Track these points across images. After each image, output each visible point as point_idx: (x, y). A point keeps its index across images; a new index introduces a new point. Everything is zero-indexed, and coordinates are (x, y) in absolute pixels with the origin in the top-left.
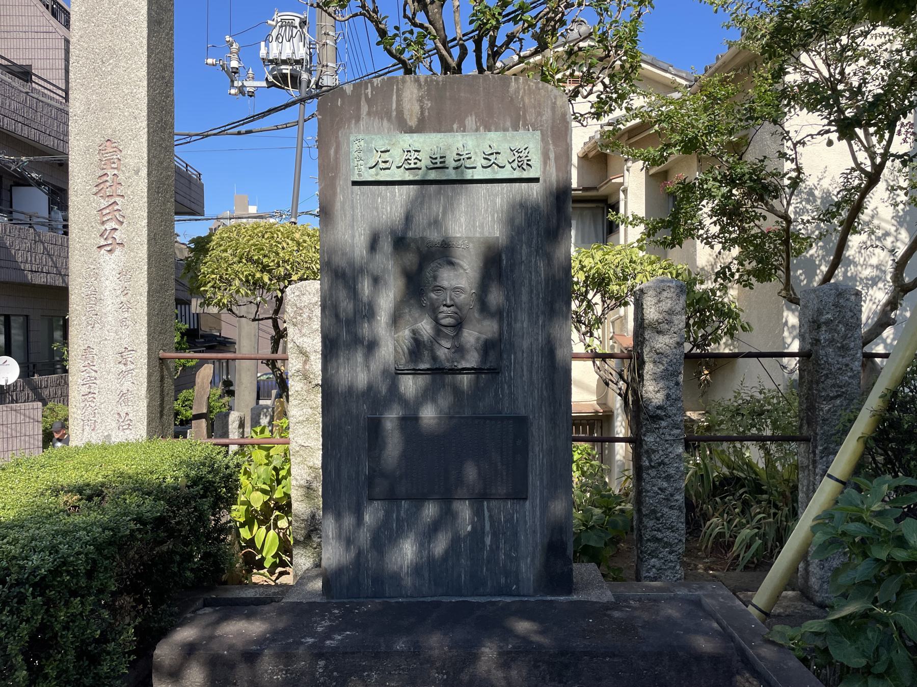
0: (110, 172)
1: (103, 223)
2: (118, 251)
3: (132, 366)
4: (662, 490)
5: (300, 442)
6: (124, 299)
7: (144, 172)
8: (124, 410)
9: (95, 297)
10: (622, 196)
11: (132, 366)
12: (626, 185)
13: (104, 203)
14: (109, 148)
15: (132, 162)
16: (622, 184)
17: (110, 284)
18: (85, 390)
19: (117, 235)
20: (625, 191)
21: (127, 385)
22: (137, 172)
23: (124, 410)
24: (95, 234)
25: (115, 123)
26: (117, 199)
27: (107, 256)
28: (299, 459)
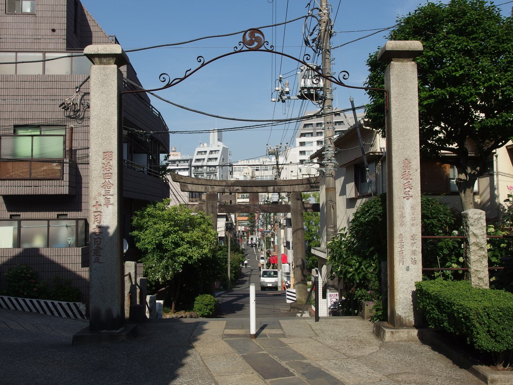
0: (407, 171)
1: (405, 189)
2: (411, 199)
3: (415, 241)
4: (500, 320)
5: (475, 268)
6: (413, 216)
7: (419, 171)
8: (413, 257)
9: (402, 216)
10: (495, 158)
11: (415, 241)
12: (497, 153)
13: (405, 182)
14: (407, 161)
15: (114, 123)
16: (495, 153)
17: (408, 211)
18: (400, 249)
19: (410, 193)
20: (497, 156)
21: (414, 248)
22: (417, 170)
23: (413, 257)
24: (402, 192)
25: (408, 153)
26: (410, 180)
27: (407, 201)
28: (474, 275)
